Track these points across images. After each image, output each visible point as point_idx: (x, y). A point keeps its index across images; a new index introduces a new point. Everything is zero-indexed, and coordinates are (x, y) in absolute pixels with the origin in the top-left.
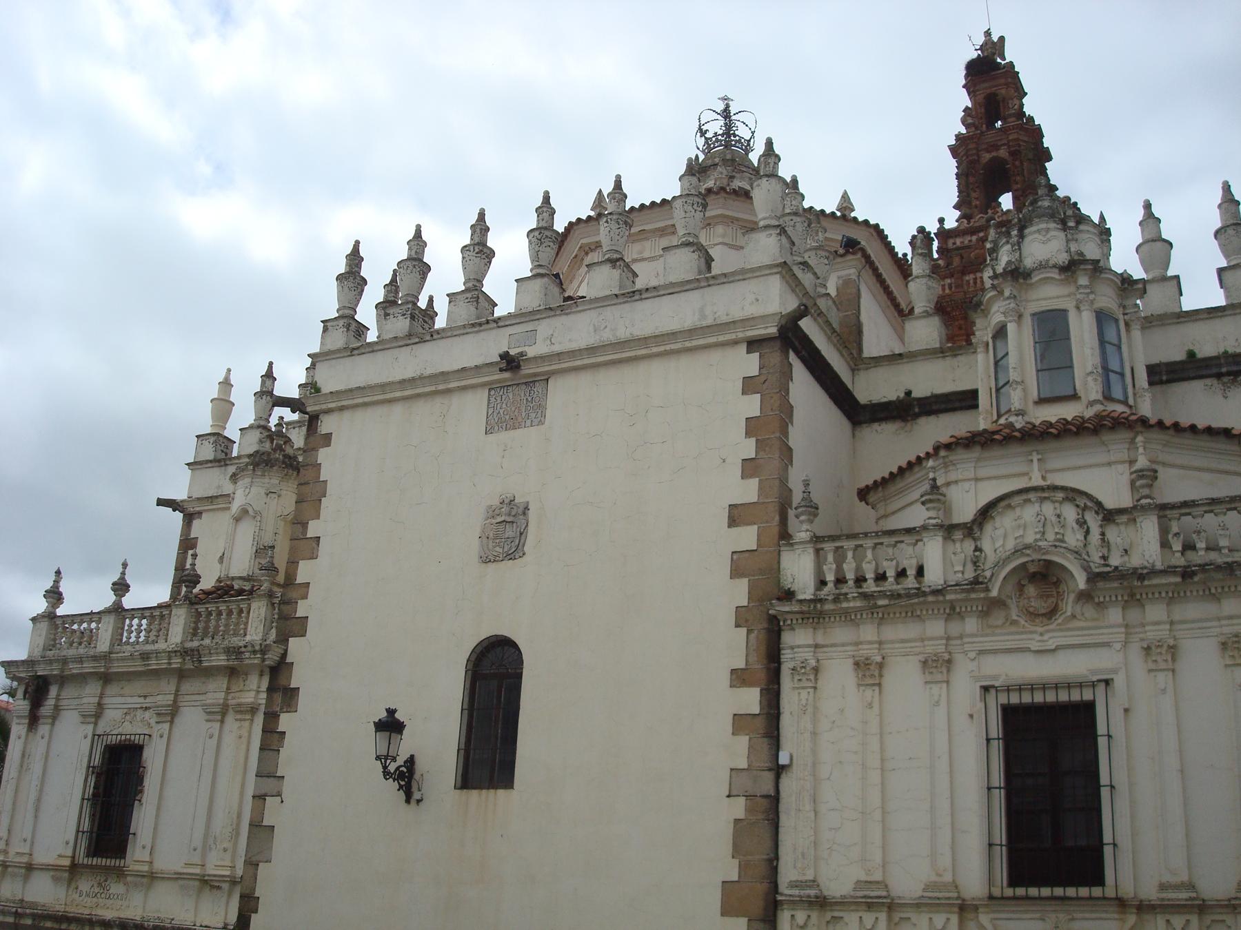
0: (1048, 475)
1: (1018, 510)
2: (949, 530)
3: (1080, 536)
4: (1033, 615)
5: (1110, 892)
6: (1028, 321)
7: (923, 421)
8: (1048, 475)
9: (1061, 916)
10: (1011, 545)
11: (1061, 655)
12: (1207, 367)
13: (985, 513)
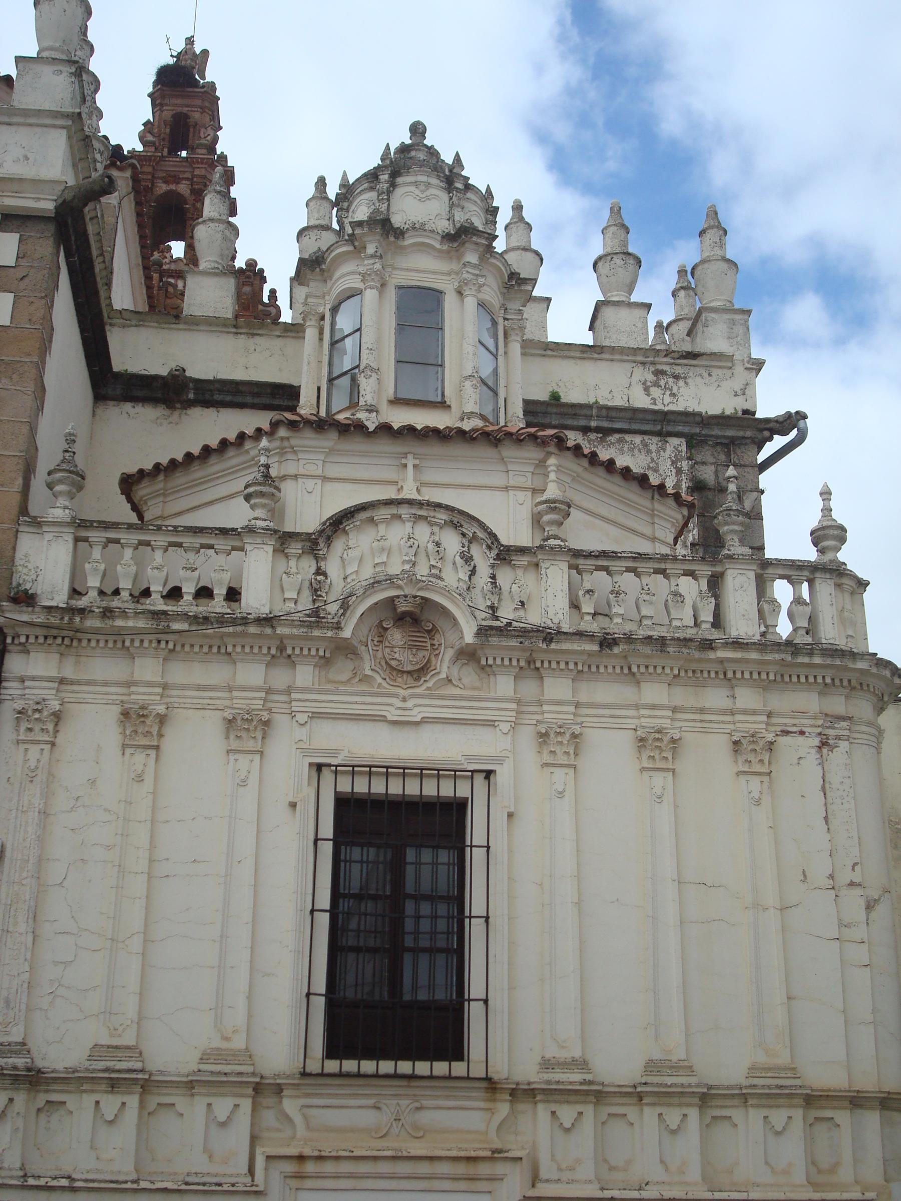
0: (424, 490)
1: (382, 528)
2: (284, 540)
3: (463, 575)
4: (395, 671)
5: (478, 1071)
6: (391, 295)
7: (197, 412)
8: (424, 490)
9: (404, 1102)
10: (367, 573)
11: (427, 731)
12: (575, 416)
13: (338, 524)
